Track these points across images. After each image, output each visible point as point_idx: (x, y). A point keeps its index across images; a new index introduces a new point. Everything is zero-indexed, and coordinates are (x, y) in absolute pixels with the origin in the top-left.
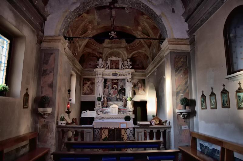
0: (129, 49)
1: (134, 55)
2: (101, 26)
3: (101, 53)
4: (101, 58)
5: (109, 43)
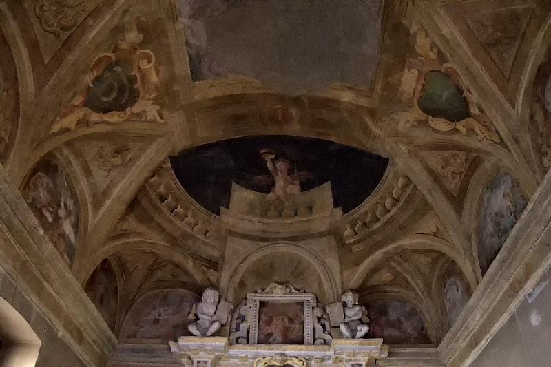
0: (351, 241)
1: (374, 271)
2: (216, 92)
3: (214, 265)
4: (215, 286)
5: (251, 209)
